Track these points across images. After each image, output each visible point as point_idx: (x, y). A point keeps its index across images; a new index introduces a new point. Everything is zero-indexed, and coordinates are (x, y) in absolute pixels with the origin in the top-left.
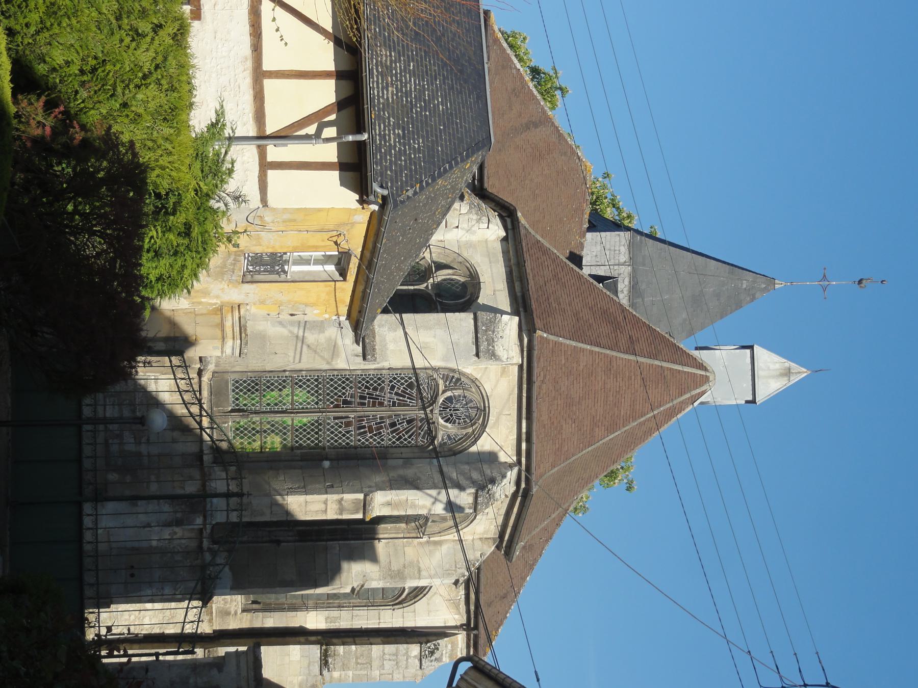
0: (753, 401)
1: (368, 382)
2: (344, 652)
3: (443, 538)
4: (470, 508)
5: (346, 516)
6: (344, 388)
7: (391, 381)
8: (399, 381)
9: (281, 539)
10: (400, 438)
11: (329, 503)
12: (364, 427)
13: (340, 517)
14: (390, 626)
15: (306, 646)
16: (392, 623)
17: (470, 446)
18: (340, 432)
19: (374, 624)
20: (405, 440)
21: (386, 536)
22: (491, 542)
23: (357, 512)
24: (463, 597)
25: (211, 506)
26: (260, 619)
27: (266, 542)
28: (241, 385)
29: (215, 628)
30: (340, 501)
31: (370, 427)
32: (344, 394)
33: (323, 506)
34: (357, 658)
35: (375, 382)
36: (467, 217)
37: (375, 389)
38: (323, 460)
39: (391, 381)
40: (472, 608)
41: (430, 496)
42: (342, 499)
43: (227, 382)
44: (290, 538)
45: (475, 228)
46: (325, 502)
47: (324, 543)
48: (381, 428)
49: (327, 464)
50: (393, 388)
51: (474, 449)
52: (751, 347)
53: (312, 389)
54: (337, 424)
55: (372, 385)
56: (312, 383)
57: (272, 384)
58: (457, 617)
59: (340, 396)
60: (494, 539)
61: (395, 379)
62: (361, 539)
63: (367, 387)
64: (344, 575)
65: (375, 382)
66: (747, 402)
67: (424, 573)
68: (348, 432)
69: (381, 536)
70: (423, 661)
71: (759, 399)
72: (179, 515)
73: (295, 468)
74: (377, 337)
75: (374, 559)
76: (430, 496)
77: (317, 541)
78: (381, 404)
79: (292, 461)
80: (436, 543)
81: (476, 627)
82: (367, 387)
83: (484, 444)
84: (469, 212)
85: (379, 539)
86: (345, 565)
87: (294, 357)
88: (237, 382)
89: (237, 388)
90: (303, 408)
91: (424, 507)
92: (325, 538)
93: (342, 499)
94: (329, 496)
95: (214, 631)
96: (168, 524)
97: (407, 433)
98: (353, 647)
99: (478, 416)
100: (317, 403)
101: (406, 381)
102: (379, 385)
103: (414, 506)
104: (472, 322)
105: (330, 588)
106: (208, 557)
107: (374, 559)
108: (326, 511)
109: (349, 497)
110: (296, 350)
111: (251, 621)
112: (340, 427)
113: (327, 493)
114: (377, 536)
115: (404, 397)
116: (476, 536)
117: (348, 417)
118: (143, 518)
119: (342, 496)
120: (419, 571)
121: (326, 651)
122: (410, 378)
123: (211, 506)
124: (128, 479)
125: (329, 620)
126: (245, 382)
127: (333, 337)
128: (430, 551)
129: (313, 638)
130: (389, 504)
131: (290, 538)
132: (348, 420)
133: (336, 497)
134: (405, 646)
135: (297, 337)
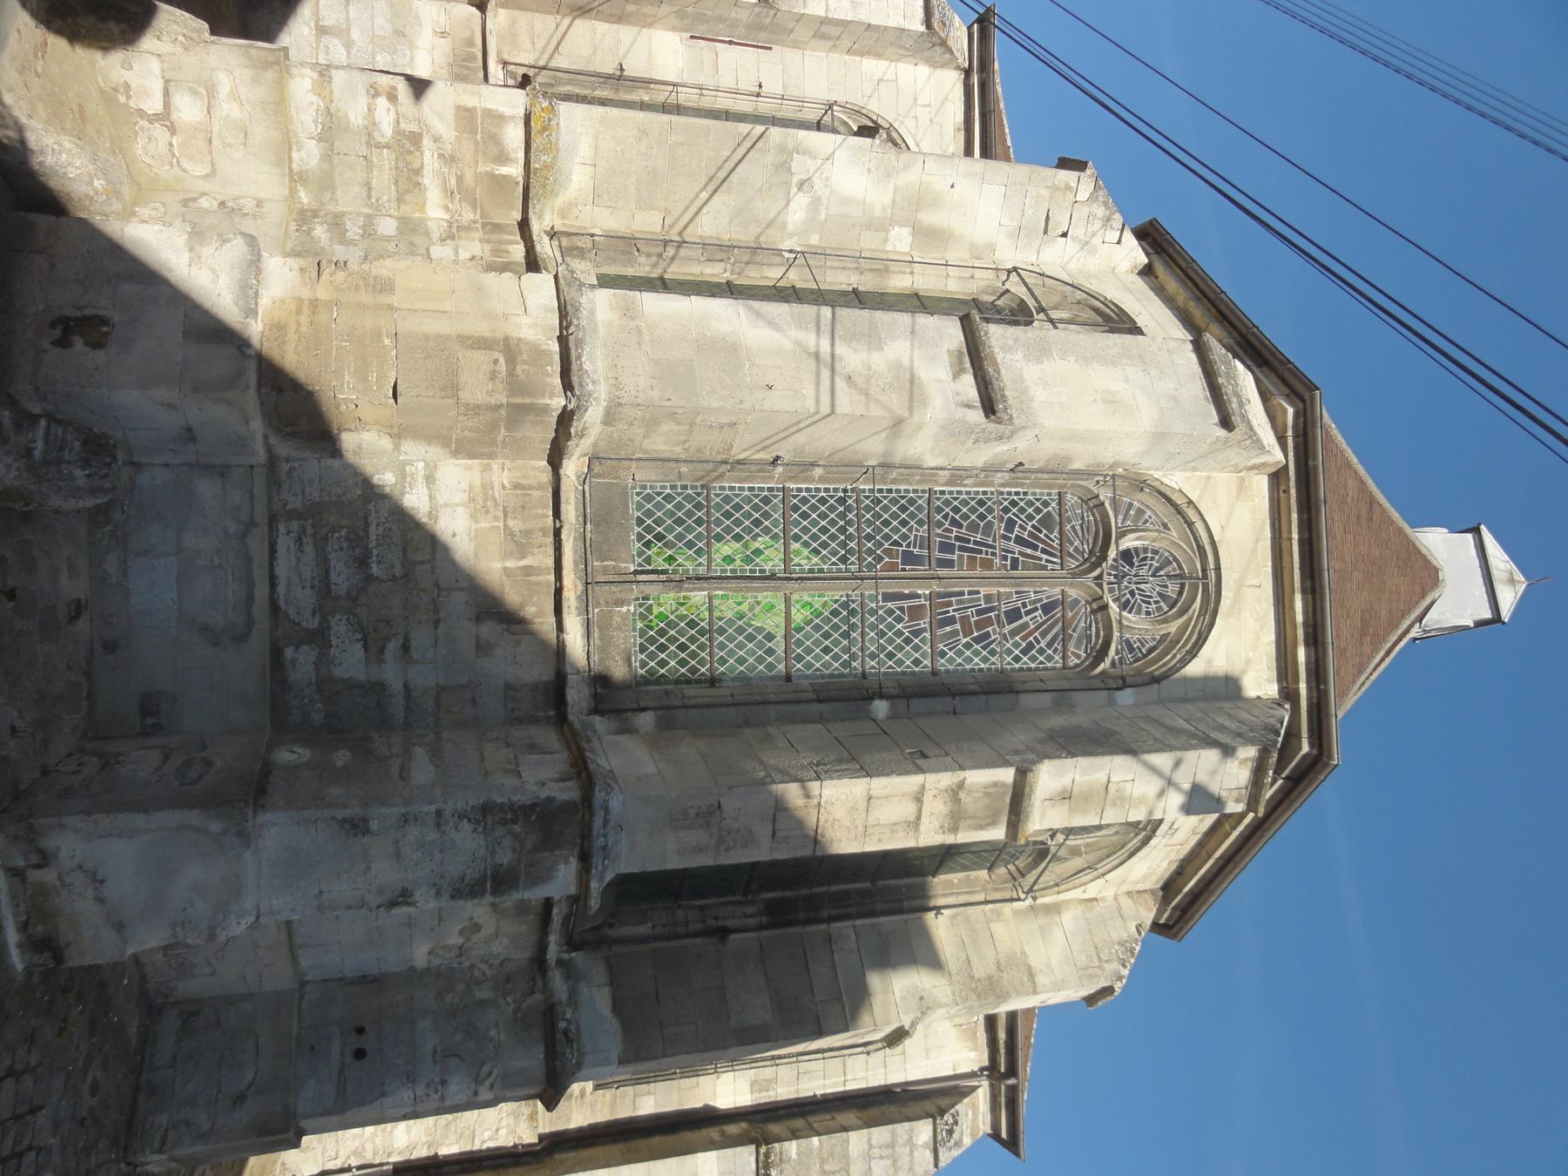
0: (1497, 619)
1: (956, 510)
2: (799, 1154)
3: (1062, 897)
4: (1237, 801)
6: (904, 523)
7: (1006, 510)
8: (1022, 510)
9: (729, 923)
10: (1030, 647)
11: (928, 797)
12: (952, 621)
13: (950, 839)
14: (862, 1085)
15: (729, 1152)
16: (866, 1078)
17: (1185, 662)
18: (899, 634)
19: (837, 1084)
20: (1041, 651)
21: (951, 900)
22: (1148, 897)
23: (993, 823)
25: (606, 823)
26: (629, 1100)
27: (695, 935)
28: (659, 506)
29: (542, 1130)
31: (965, 621)
32: (905, 537)
33: (909, 809)
34: (823, 1162)
35: (973, 510)
36: (1086, 210)
37: (973, 527)
38: (871, 698)
39: (1006, 510)
40: (1002, 1036)
41: (1153, 769)
42: (961, 785)
43: (624, 492)
44: (751, 922)
45: (1096, 241)
46: (919, 798)
47: (823, 927)
48: (989, 622)
49: (881, 708)
50: (1010, 525)
51: (1195, 668)
52: (1476, 531)
53: (833, 523)
54: (890, 612)
55: (965, 517)
56: (832, 509)
57: (738, 507)
58: (973, 1055)
59: (896, 543)
60: (1152, 892)
61: (1014, 504)
62: (901, 912)
63: (954, 523)
64: (877, 1001)
65: (973, 510)
66: (1480, 624)
67: (1041, 980)
68: (916, 633)
69: (940, 902)
70: (941, 1150)
71: (1506, 615)
72: (505, 857)
73: (806, 721)
74: (1003, 371)
75: (933, 962)
76: (1153, 769)
77: (809, 922)
78: (987, 564)
79: (798, 702)
80: (1055, 909)
81: (1012, 1071)
82: (954, 523)
83: (1213, 659)
84: (1093, 198)
85: (938, 909)
86: (875, 980)
87: (817, 400)
88: (649, 498)
89: (649, 514)
90: (811, 571)
91: (1142, 800)
92: (825, 914)
95: (542, 1138)
96: (468, 890)
97: (1044, 635)
98: (815, 1140)
99: (1198, 589)
100: (844, 560)
101: (1038, 511)
102: (982, 517)
104: (1193, 357)
105: (848, 1034)
106: (558, 981)
107: (933, 962)
109: (978, 778)
110: (818, 383)
111: (613, 1106)
112: (899, 620)
113: (921, 770)
114: (933, 903)
115: (1035, 548)
116: (1125, 888)
117: (919, 596)
118: (386, 874)
119: (961, 775)
120: (1031, 975)
121: (767, 1155)
122: (1046, 504)
123: (606, 823)
124: (342, 757)
125: (756, 1087)
126: (669, 498)
127: (905, 361)
128: (1041, 928)
129: (733, 1129)
130: (1066, 796)
131: (751, 922)
132: (915, 602)
133: (945, 779)
134: (907, 1125)
135: (817, 356)
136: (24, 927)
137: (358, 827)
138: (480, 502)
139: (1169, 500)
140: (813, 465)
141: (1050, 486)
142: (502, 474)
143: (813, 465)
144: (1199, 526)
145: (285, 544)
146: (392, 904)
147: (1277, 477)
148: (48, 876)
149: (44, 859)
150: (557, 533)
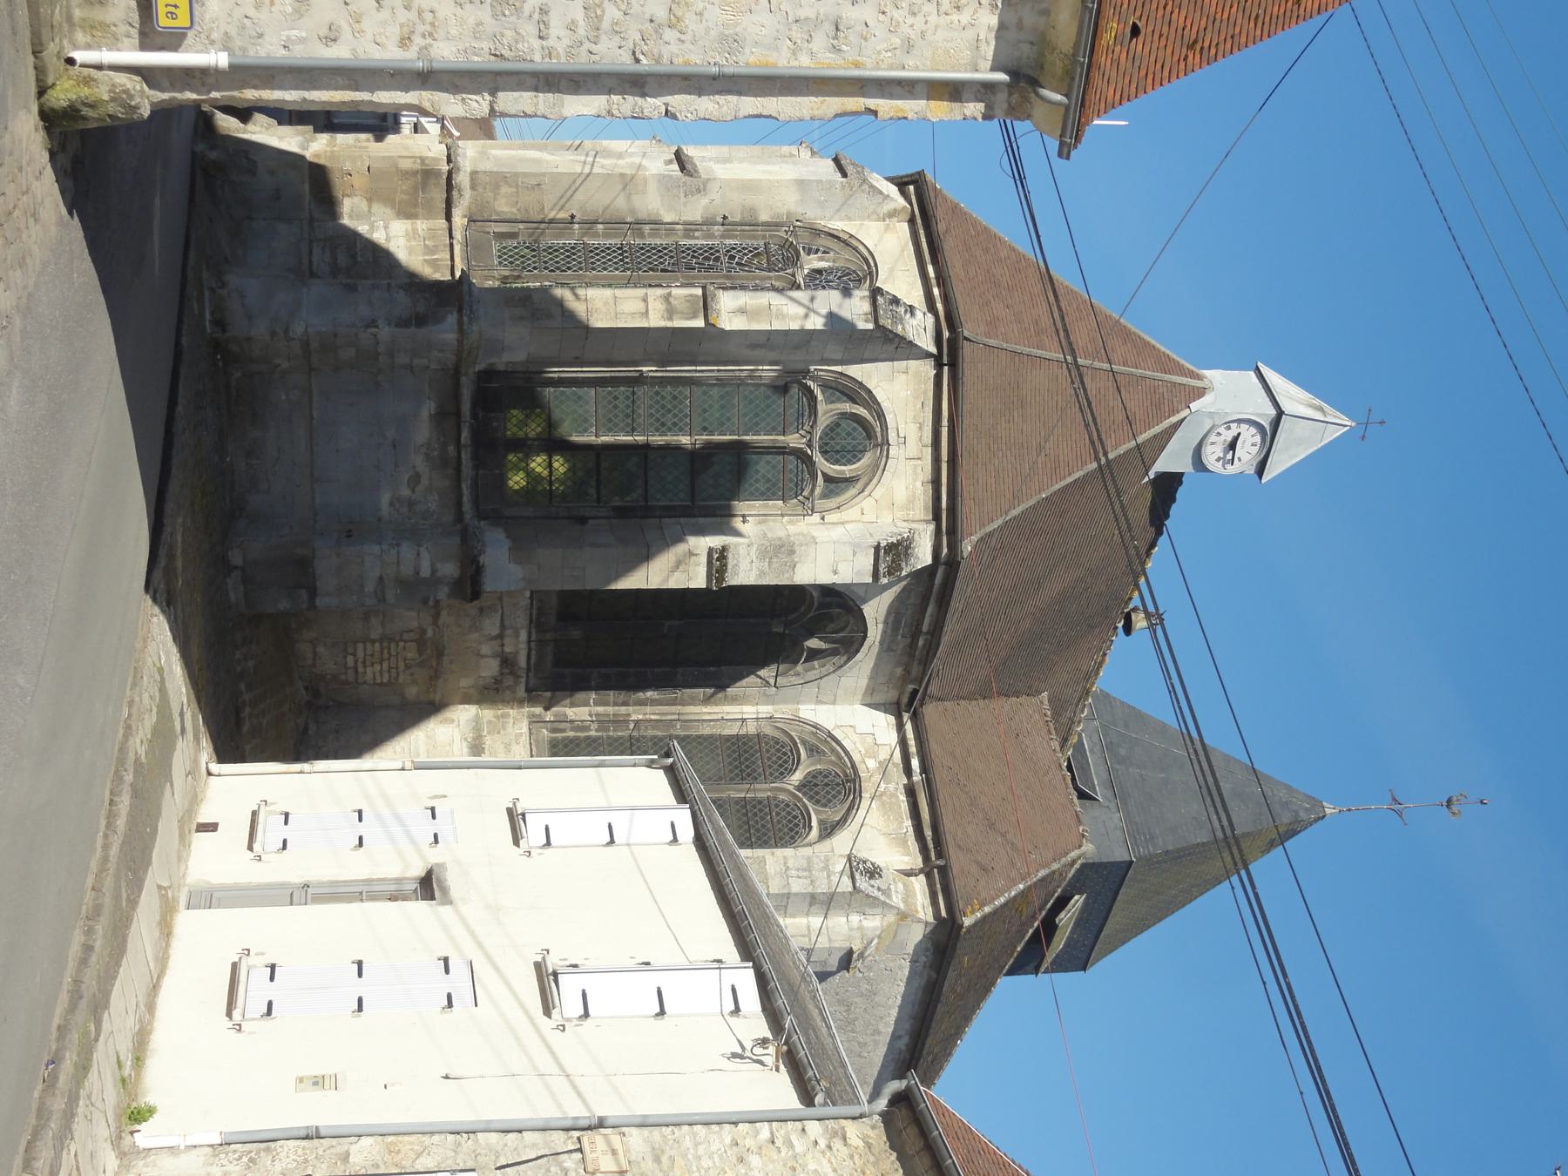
5: (679, 323)
11: (650, 300)
13: (669, 324)
23: (694, 317)
24: (911, 829)
30: (667, 298)
33: (641, 306)
40: (928, 833)
46: (645, 300)
58: (906, 859)
72: (421, 309)
93: (669, 294)
94: (651, 291)
96: (403, 323)
103: (781, 316)
108: (646, 314)
130: (742, 311)
133: (659, 291)
136: (212, 313)
137: (351, 288)
138: (412, 235)
139: (838, 238)
140: (596, 222)
141: (755, 238)
142: (421, 225)
143: (596, 222)
144: (861, 248)
145: (315, 251)
146: (368, 326)
147: (912, 221)
148: (224, 292)
149: (223, 285)
150: (451, 245)
